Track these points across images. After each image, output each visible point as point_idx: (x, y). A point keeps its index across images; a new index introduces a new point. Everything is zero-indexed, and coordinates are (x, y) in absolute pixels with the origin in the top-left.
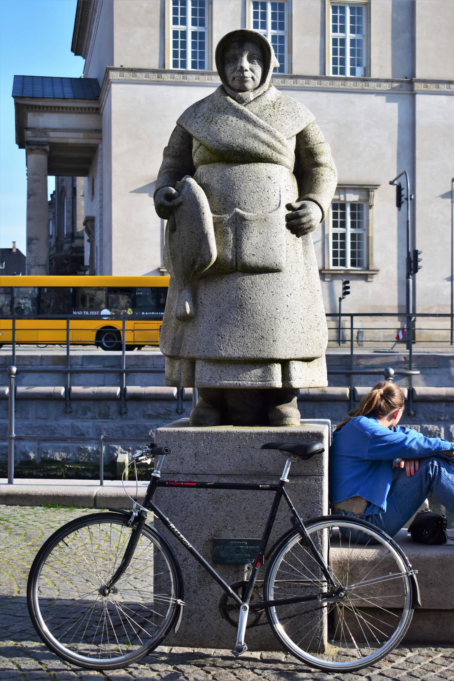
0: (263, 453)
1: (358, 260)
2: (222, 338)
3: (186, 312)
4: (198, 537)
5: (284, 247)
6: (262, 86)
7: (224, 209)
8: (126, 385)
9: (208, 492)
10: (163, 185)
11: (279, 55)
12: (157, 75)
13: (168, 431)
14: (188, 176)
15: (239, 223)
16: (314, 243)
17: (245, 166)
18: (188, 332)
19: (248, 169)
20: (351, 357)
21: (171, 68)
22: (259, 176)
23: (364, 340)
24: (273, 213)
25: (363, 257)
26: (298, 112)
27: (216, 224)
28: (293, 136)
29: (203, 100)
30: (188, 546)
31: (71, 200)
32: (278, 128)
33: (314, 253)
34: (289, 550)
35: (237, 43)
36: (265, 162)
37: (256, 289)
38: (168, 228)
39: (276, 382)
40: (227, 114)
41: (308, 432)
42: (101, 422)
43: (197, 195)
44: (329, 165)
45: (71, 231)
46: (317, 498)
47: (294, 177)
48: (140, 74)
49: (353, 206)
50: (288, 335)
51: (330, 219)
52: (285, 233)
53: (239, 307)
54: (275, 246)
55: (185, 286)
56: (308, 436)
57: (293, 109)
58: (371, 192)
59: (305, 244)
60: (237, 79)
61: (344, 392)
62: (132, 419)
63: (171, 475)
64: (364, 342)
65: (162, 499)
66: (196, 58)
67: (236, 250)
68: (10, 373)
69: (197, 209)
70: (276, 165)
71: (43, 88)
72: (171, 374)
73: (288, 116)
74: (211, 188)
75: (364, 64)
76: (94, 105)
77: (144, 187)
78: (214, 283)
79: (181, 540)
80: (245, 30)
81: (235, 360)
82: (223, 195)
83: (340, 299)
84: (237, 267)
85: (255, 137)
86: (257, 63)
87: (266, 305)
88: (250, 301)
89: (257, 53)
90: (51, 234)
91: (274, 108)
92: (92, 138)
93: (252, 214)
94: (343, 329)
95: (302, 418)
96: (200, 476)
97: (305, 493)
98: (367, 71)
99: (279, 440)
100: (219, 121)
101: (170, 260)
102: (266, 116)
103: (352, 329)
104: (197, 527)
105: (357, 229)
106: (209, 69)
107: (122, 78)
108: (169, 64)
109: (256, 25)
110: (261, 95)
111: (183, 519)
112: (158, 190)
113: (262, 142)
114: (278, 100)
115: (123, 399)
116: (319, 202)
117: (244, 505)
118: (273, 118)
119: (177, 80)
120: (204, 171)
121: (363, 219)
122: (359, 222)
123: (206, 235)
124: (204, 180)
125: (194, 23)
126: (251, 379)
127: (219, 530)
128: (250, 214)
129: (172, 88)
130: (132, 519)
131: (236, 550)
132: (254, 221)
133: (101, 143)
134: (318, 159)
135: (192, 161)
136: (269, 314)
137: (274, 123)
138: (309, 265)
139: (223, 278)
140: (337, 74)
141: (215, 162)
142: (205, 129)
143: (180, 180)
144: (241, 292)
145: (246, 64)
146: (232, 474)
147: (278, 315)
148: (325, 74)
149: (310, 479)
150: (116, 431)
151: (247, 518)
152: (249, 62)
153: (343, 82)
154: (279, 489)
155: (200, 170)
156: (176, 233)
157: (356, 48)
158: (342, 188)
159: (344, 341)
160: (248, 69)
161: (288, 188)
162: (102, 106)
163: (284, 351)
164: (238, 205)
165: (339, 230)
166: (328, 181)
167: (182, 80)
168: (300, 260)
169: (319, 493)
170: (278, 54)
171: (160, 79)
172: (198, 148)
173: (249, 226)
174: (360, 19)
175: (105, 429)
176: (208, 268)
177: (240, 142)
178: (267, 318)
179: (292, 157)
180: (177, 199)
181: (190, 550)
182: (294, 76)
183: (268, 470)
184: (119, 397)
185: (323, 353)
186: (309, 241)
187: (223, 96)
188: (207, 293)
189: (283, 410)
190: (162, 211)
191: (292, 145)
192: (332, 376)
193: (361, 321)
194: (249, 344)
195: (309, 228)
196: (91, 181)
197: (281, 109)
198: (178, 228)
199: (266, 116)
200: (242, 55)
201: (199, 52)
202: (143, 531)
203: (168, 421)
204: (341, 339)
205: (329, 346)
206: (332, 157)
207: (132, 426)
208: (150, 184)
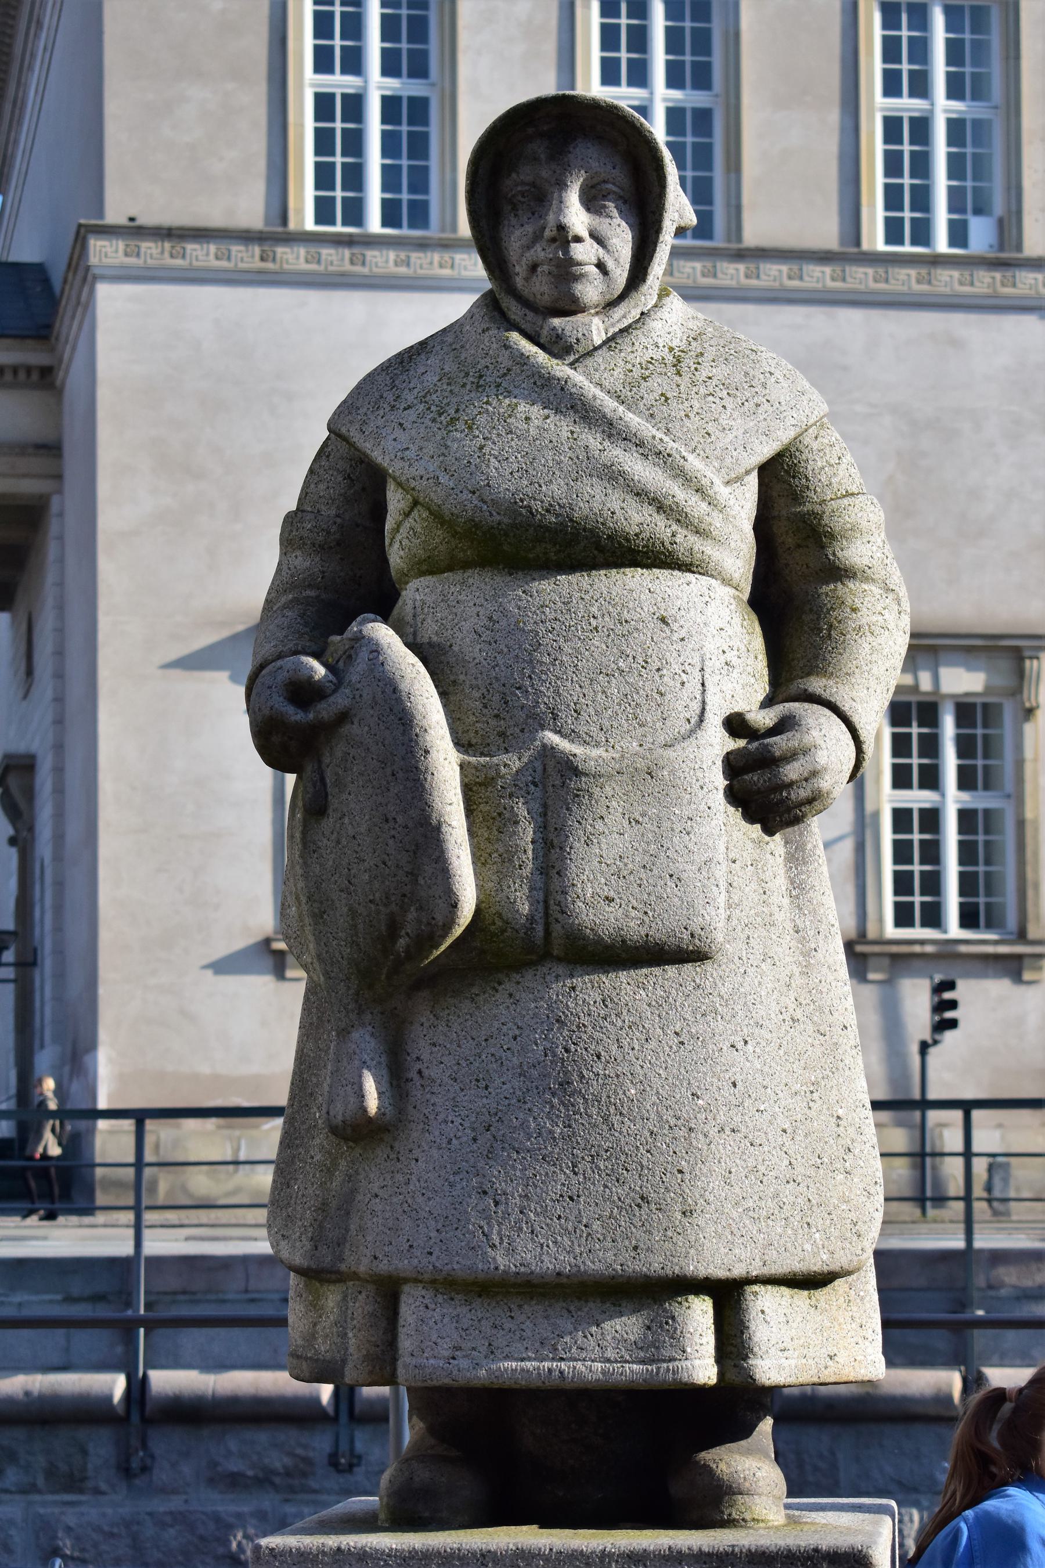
1: (988, 905)
2: (496, 1204)
3: (365, 1110)
6: (634, 295)
7: (502, 734)
8: (148, 1365)
10: (280, 648)
11: (695, 179)
12: (257, 250)
13: (298, 1549)
14: (371, 616)
15: (558, 785)
16: (827, 845)
17: (574, 578)
18: (374, 1179)
19: (587, 592)
20: (965, 1257)
21: (310, 225)
22: (626, 615)
23: (1012, 1194)
24: (678, 747)
25: (1003, 895)
26: (764, 386)
28: (748, 472)
29: (423, 344)
32: (693, 445)
33: (829, 892)
35: (546, 141)
36: (648, 567)
37: (620, 1023)
38: (300, 804)
39: (697, 1362)
40: (509, 394)
41: (816, 1550)
42: (55, 1503)
43: (404, 686)
44: (879, 573)
47: (754, 617)
48: (196, 246)
49: (966, 711)
50: (737, 1190)
51: (883, 760)
52: (721, 818)
53: (558, 1080)
55: (360, 1012)
57: (747, 374)
58: (1027, 663)
59: (796, 858)
60: (545, 268)
61: (944, 1388)
62: (165, 1491)
64: (1012, 1204)
66: (399, 190)
69: (404, 733)
70: (690, 576)
72: (311, 1337)
73: (729, 402)
75: (999, 205)
77: (212, 648)
78: (467, 1002)
80: (573, 97)
81: (544, 1285)
82: (496, 685)
83: (924, 1047)
84: (549, 943)
85: (613, 476)
86: (615, 213)
87: (657, 1083)
89: (617, 176)
91: (679, 374)
92: (25, 476)
94: (934, 1155)
95: (790, 1494)
98: (1010, 229)
100: (482, 420)
101: (307, 921)
102: (650, 399)
103: (968, 1154)
105: (981, 793)
106: (443, 230)
107: (132, 261)
108: (300, 211)
109: (610, 75)
110: (630, 326)
112: (261, 667)
113: (638, 494)
115: (135, 1418)
116: (846, 707)
118: (677, 409)
119: (331, 268)
120: (429, 600)
121: (1000, 756)
122: (986, 768)
123: (438, 829)
124: (429, 631)
125: (390, 67)
126: (601, 1352)
128: (595, 752)
129: (314, 298)
133: (60, 491)
134: (840, 554)
135: (386, 561)
136: (668, 1116)
137: (677, 424)
138: (811, 933)
139: (500, 983)
140: (900, 242)
141: (466, 565)
142: (430, 448)
143: (341, 633)
144: (566, 1033)
145: (577, 217)
148: (858, 243)
150: (112, 1535)
152: (588, 210)
153: (924, 271)
155: (415, 593)
156: (328, 824)
157: (969, 150)
158: (926, 647)
159: (941, 1200)
160: (584, 234)
161: (731, 656)
162: (61, 361)
163: (723, 1251)
164: (553, 720)
165: (917, 798)
166: (877, 630)
167: (347, 267)
168: (780, 917)
170: (689, 174)
171: (270, 265)
172: (407, 515)
173: (591, 795)
174: (980, 49)
175: (69, 1529)
176: (443, 948)
177: (557, 493)
178: (661, 1128)
179: (743, 546)
180: (332, 699)
182: (748, 249)
184: (121, 1411)
185: (865, 1256)
186: (809, 846)
188: (441, 1040)
189: (723, 1466)
190: (276, 742)
191: (742, 503)
192: (896, 1332)
193: (1000, 1126)
194: (596, 1225)
195: (810, 801)
196: (24, 627)
197: (704, 373)
198: (334, 802)
201: (410, 167)
203: (299, 1497)
204: (929, 1193)
205: (887, 1219)
206: (887, 547)
207: (168, 1519)
208: (235, 638)
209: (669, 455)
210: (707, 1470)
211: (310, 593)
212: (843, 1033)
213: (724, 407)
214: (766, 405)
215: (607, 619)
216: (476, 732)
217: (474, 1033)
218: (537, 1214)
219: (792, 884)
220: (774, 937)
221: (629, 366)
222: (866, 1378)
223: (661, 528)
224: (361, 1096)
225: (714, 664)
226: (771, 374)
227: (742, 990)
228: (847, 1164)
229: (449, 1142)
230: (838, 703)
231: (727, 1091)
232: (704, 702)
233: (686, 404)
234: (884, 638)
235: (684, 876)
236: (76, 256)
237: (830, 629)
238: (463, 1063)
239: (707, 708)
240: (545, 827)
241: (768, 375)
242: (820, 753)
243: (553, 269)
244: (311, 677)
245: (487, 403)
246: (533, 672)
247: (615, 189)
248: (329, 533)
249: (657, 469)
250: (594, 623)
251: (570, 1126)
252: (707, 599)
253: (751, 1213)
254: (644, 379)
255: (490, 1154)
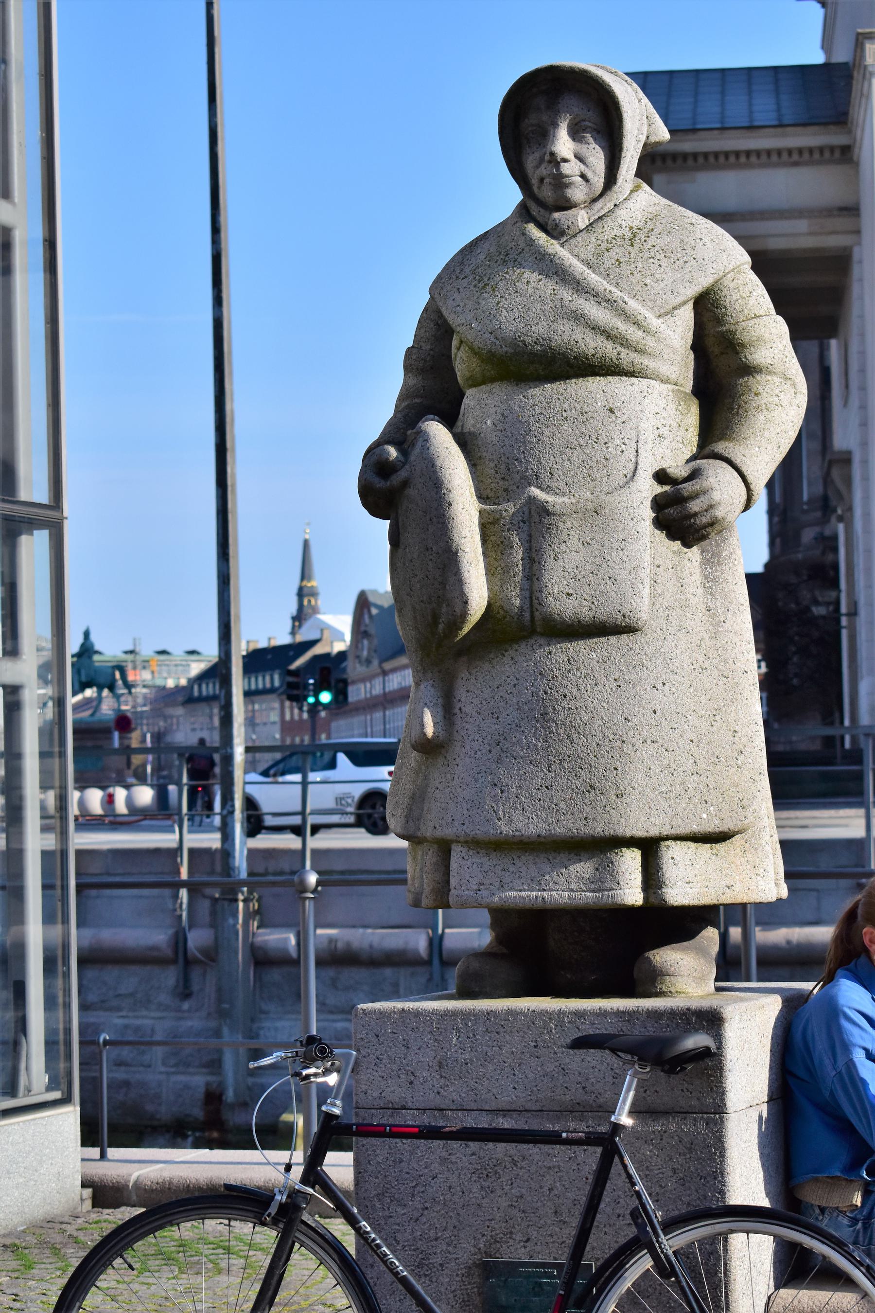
0: (589, 1059)
2: (502, 792)
4: (450, 1257)
5: (648, 570)
6: (609, 193)
7: (506, 490)
9: (469, 1151)
15: (536, 522)
17: (555, 386)
22: (586, 408)
24: (615, 493)
27: (487, 527)
30: (398, 1273)
31: (819, 403)
32: (634, 293)
34: (629, 1285)
37: (579, 674)
39: (627, 891)
40: (521, 266)
41: (688, 1009)
43: (438, 463)
44: (779, 367)
45: (819, 490)
46: (711, 1167)
52: (647, 539)
53: (541, 716)
54: (621, 572)
56: (687, 1019)
63: (389, 1112)
65: (370, 1168)
67: (531, 586)
68: (302, 888)
69: (436, 494)
70: (633, 380)
71: (696, 102)
74: (480, 443)
76: (836, 138)
79: (383, 1257)
81: (532, 843)
82: (503, 459)
84: (527, 626)
85: (577, 317)
86: (591, 140)
88: (565, 703)
89: (591, 116)
91: (632, 245)
93: (565, 499)
96: (450, 1113)
97: (685, 1155)
99: (624, 1029)
100: (501, 285)
102: (608, 264)
104: (447, 1234)
111: (416, 1215)
113: (593, 329)
114: (649, 223)
116: (737, 461)
117: (548, 1181)
118: (625, 269)
126: (566, 886)
127: (496, 1242)
128: (559, 500)
130: (273, 1210)
131: (533, 1289)
132: (570, 515)
133: (859, 243)
134: (749, 357)
139: (506, 651)
141: (492, 380)
146: (521, 1109)
147: (631, 733)
149: (695, 1119)
151: (556, 1212)
152: (574, 140)
154: (608, 1142)
160: (570, 156)
161: (664, 431)
166: (772, 407)
168: (693, 601)
169: (715, 1154)
173: (557, 527)
177: (541, 330)
180: (399, 473)
181: (404, 1281)
183: (602, 1100)
187: (519, 224)
194: (562, 805)
195: (712, 524)
197: (651, 243)
199: (608, 264)
200: (555, 125)
202: (298, 1235)
209: (615, 301)
210: (649, 960)
211: (417, 400)
212: (743, 676)
213: (660, 265)
214: (693, 262)
215: (573, 412)
216: (491, 489)
217: (491, 683)
218: (526, 798)
219: (706, 578)
220: (688, 615)
221: (599, 242)
222: (758, 901)
223: (609, 350)
224: (422, 725)
225: (649, 436)
226: (701, 239)
227: (662, 650)
228: (739, 762)
230: (732, 459)
231: (649, 714)
232: (637, 463)
233: (633, 266)
234: (777, 413)
235: (618, 577)
236: (858, 59)
237: (738, 409)
238: (484, 703)
239: (639, 467)
240: (530, 549)
241: (698, 241)
242: (715, 493)
243: (552, 180)
244: (387, 459)
245: (507, 273)
246: (526, 449)
247: (590, 124)
248: (425, 361)
249: (606, 311)
250: (565, 414)
251: (547, 741)
252: (645, 394)
253: (664, 795)
254: (608, 250)
255: (498, 761)
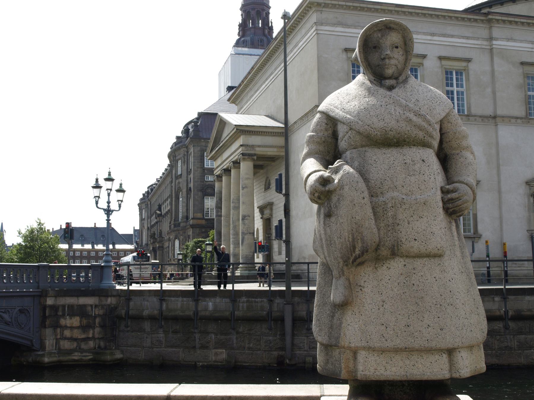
90: (179, 173)
156: (333, 219)
229: (371, 310)
235: (435, 233)
